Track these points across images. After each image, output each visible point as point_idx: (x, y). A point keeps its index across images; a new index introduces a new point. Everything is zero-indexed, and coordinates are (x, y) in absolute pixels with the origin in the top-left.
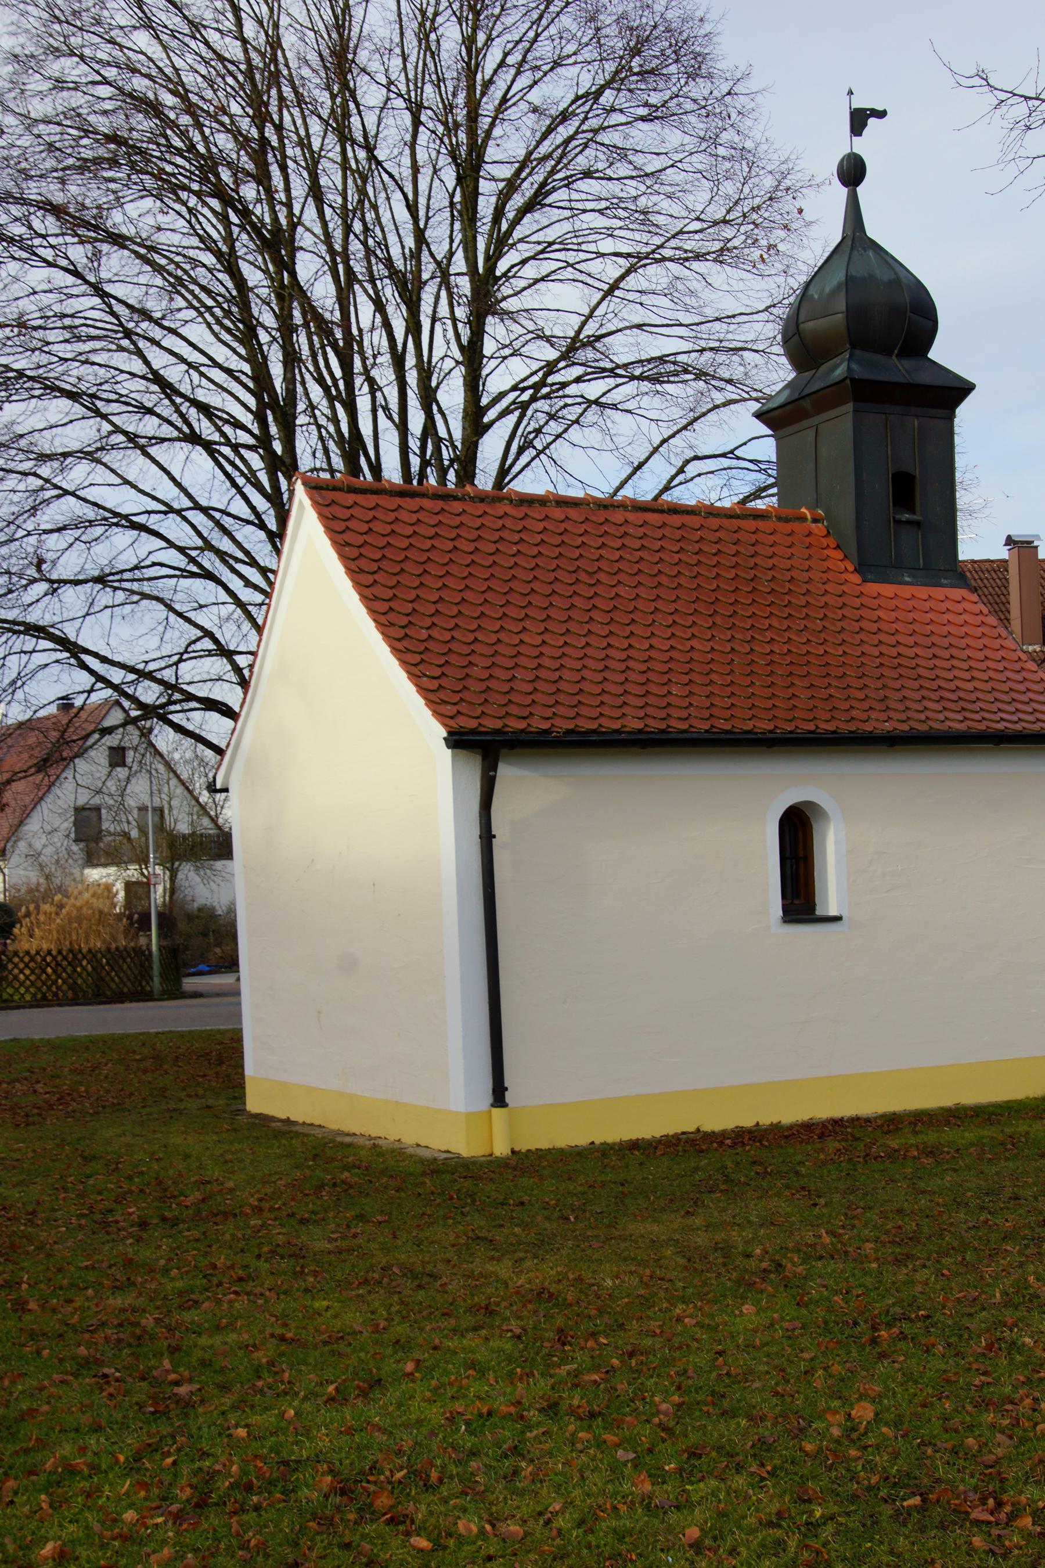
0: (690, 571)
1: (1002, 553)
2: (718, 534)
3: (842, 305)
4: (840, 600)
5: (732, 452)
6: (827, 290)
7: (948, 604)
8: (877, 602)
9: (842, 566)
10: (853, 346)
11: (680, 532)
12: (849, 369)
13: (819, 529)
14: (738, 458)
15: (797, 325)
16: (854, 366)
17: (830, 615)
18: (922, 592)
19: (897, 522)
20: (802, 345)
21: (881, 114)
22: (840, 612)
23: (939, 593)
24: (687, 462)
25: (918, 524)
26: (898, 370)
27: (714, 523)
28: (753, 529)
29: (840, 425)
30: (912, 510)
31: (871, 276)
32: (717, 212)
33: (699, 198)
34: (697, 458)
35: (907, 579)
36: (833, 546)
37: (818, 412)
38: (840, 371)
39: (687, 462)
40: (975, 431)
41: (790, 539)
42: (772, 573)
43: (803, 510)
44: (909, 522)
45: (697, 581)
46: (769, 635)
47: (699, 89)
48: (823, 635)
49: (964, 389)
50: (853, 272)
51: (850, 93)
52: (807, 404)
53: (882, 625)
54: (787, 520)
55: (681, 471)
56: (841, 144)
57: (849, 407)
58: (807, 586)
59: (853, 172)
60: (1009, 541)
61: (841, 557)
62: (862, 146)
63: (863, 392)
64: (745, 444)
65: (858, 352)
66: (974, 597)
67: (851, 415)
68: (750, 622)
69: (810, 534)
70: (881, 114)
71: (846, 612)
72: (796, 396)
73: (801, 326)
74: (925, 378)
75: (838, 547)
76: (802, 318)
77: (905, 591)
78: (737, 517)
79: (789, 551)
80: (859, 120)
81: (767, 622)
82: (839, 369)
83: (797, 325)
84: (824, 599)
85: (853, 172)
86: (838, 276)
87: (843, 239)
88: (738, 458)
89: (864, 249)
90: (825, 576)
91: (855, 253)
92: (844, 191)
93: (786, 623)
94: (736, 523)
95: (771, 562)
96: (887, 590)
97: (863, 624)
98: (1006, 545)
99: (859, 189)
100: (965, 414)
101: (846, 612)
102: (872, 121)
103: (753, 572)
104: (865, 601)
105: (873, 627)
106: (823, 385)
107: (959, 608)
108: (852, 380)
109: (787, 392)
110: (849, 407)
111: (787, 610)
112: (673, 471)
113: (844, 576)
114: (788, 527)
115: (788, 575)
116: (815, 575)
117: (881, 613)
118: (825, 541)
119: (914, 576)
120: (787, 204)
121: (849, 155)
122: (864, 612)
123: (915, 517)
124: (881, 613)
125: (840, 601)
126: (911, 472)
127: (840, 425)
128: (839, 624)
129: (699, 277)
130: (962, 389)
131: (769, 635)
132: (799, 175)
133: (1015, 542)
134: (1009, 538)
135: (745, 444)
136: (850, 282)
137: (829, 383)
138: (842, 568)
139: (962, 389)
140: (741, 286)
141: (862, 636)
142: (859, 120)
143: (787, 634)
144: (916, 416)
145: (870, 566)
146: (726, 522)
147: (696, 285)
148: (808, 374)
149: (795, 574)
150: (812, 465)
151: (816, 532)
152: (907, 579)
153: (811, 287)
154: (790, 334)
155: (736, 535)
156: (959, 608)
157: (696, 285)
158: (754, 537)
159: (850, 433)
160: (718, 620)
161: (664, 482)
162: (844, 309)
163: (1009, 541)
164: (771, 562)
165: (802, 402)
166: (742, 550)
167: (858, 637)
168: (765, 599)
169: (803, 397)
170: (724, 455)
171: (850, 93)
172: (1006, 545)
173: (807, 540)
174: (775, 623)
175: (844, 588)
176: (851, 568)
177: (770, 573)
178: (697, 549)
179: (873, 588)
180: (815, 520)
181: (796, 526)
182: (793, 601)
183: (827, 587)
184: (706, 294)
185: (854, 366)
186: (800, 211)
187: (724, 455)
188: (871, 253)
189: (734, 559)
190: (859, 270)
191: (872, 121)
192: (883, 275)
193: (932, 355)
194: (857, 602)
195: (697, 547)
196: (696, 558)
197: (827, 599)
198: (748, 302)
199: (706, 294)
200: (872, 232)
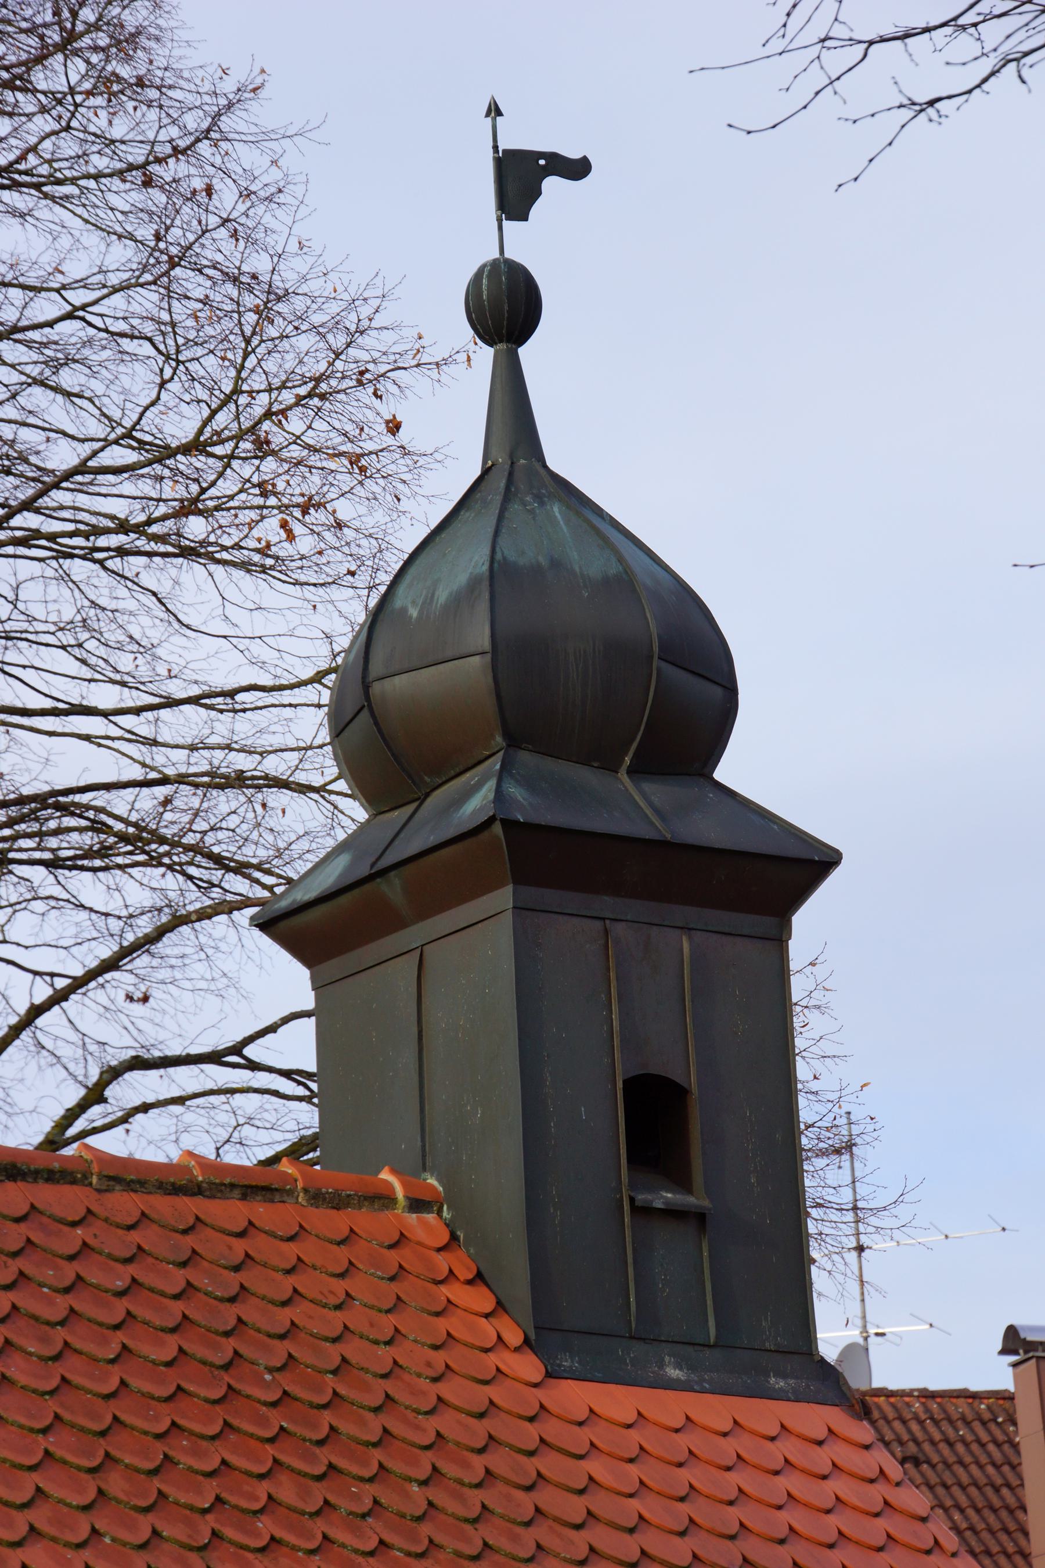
0: (44, 1340)
1: (997, 1375)
2: (135, 1237)
3: (480, 636)
4: (481, 1429)
5: (237, 1049)
6: (442, 596)
7: (788, 1448)
8: (586, 1434)
9: (488, 1330)
10: (514, 741)
11: (23, 1228)
12: (499, 795)
13: (427, 1228)
14: (253, 1066)
15: (366, 686)
16: (515, 791)
17: (450, 1469)
18: (715, 1410)
19: (642, 1211)
20: (384, 739)
21: (577, 169)
22: (479, 1462)
23: (762, 1414)
24: (113, 1074)
25: (700, 1218)
26: (632, 805)
27: (125, 1205)
28: (240, 1225)
29: (479, 946)
30: (683, 1182)
31: (556, 564)
32: (179, 427)
33: (129, 383)
34: (139, 1063)
35: (674, 1373)
36: (465, 1273)
37: (425, 910)
38: (478, 804)
39: (113, 1074)
40: (857, 998)
41: (343, 1254)
42: (287, 1346)
43: (385, 1175)
44: (672, 1213)
45: (58, 1369)
46: (266, 1526)
47: (131, 126)
48: (426, 1529)
49: (814, 864)
50: (507, 550)
51: (494, 111)
52: (393, 889)
53: (600, 1503)
54: (338, 1202)
55: (95, 1095)
56: (475, 236)
57: (504, 897)
58: (388, 1386)
59: (506, 309)
60: (1014, 1341)
61: (489, 1306)
62: (526, 243)
63: (540, 858)
64: (272, 1029)
65: (525, 757)
66: (863, 1432)
67: (508, 918)
68: (211, 1489)
69: (401, 1241)
70: (577, 169)
71: (498, 1461)
72: (364, 871)
73: (376, 688)
74: (706, 830)
75: (479, 1278)
76: (377, 667)
77: (668, 1407)
78: (194, 1190)
79: (340, 1286)
80: (520, 181)
81: (262, 1489)
82: (476, 800)
83: (366, 686)
84: (433, 1424)
85: (506, 309)
86: (471, 559)
87: (486, 472)
88: (253, 1066)
89: (539, 498)
90: (440, 1358)
91: (515, 507)
92: (485, 355)
93: (320, 1492)
94: (190, 1206)
95: (283, 1317)
96: (617, 1401)
97: (545, 1497)
98: (1004, 1351)
99: (522, 351)
100: (811, 925)
101: (498, 1461)
102: (552, 185)
103: (232, 1343)
104: (551, 1429)
105: (575, 1508)
106: (433, 840)
107: (821, 1459)
108: (509, 825)
109: (343, 861)
110: (504, 897)
111: (326, 1455)
112: (74, 1095)
113: (493, 1359)
114: (340, 1222)
115: (333, 1354)
116: (412, 1355)
117: (595, 1467)
118: (442, 1263)
119: (692, 1368)
120: (359, 407)
121: (495, 263)
122: (548, 1464)
123: (691, 1200)
124: (595, 1467)
125: (481, 1429)
126: (677, 1076)
127: (479, 946)
128: (477, 1497)
129: (150, 601)
130: (807, 865)
131: (266, 1526)
132: (388, 336)
133: (1030, 1346)
134: (1011, 1332)
135: (272, 1029)
136: (500, 575)
137: (451, 833)
138: (488, 1334)
139: (807, 865)
140: (257, 624)
141: (540, 1532)
142: (520, 181)
143: (320, 1526)
144: (687, 929)
145: (560, 1337)
146: (161, 1205)
147: (147, 625)
148: (399, 815)
149: (351, 1349)
150: (408, 1057)
151: (420, 1235)
152: (674, 1373)
153: (401, 590)
154: (349, 711)
155: (189, 1240)
156: (821, 1459)
157: (147, 625)
158: (240, 1246)
159: (508, 966)
160: (116, 1484)
161: (47, 1126)
162: (486, 643)
163: (1014, 1341)
164: (283, 1317)
165: (381, 885)
166: (203, 1282)
167: (529, 1537)
168: (263, 1422)
169: (383, 872)
170: (215, 1058)
171: (494, 111)
172: (1004, 1351)
173: (394, 1257)
174: (286, 1492)
175: (491, 1392)
176: (514, 1337)
177: (281, 1350)
178: (69, 1279)
179: (575, 1396)
180: (417, 1205)
181: (361, 1219)
182: (344, 1427)
183: (444, 1389)
184: (175, 649)
185: (515, 791)
186: (394, 427)
187: (215, 1058)
188: (556, 509)
189: (177, 1308)
190: (524, 548)
191: (552, 185)
192: (591, 563)
193: (721, 774)
194: (530, 1435)
195: (69, 1272)
196: (63, 1302)
197: (445, 1423)
198: (262, 640)
199: (175, 649)
200: (559, 458)
